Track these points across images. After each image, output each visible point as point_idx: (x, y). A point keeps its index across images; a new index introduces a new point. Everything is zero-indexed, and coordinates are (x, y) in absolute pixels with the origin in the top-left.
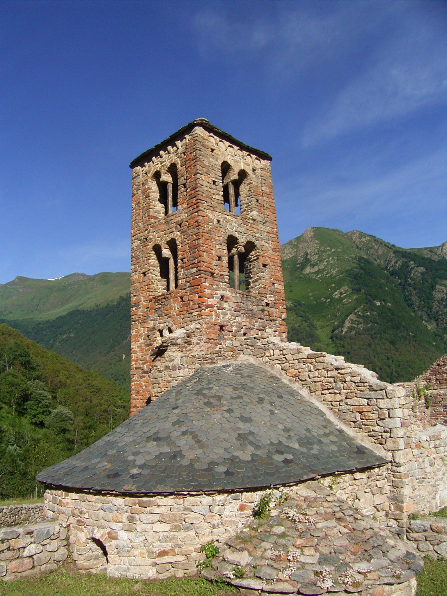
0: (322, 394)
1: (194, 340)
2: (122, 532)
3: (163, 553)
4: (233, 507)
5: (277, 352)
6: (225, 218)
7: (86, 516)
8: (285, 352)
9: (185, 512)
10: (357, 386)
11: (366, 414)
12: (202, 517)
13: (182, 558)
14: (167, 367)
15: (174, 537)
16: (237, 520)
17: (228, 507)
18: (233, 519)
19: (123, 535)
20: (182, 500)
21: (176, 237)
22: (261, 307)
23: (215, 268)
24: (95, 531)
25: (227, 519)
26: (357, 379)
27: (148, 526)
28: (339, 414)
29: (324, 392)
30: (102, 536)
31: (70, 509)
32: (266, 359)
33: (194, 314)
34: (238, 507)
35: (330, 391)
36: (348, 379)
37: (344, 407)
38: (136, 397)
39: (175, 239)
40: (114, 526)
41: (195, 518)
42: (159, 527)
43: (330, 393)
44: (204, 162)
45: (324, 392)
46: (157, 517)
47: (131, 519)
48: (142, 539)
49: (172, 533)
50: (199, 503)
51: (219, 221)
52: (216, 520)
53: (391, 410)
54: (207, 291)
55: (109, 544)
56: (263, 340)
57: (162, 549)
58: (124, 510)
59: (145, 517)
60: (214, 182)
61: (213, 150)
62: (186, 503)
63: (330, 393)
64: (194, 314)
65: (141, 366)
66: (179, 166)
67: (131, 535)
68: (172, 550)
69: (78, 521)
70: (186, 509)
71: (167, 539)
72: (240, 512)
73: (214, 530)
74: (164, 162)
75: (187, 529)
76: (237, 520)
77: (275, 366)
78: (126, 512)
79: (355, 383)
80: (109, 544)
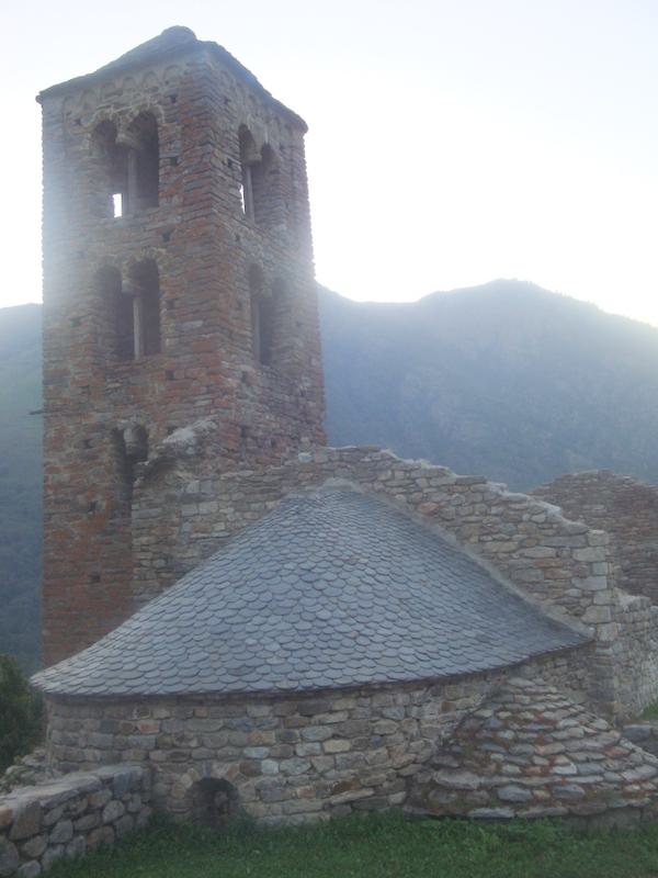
0: (480, 541)
1: (209, 450)
2: (269, 761)
3: (343, 787)
4: (433, 707)
5: (399, 474)
6: (246, 232)
7: (194, 743)
8: (414, 474)
9: (374, 719)
10: (540, 528)
11: (556, 571)
12: (397, 725)
13: (369, 792)
14: (171, 499)
15: (357, 760)
16: (439, 726)
17: (427, 708)
18: (434, 726)
19: (271, 766)
20: (369, 700)
21: (156, 257)
22: (293, 398)
23: (234, 322)
24: (215, 766)
25: (427, 726)
26: (540, 518)
27: (317, 746)
28: (508, 572)
29: (485, 538)
30: (229, 773)
31: (153, 737)
32: (378, 486)
33: (199, 403)
34: (439, 706)
35: (495, 536)
36: (525, 517)
37: (515, 560)
38: (56, 557)
39: (153, 261)
40: (253, 752)
41: (389, 727)
42: (331, 746)
43: (494, 540)
44: (217, 123)
45: (485, 538)
46: (329, 731)
47: (287, 739)
48: (306, 767)
49: (356, 753)
50: (392, 703)
51: (238, 238)
52: (414, 730)
53: (595, 565)
54: (226, 364)
55: (244, 785)
56: (374, 454)
57: (340, 780)
58: (273, 725)
59: (309, 732)
60: (230, 163)
61: (227, 101)
62: (375, 705)
63: (494, 540)
64: (199, 403)
65: (71, 498)
66: (162, 120)
67: (287, 765)
68: (356, 779)
69: (176, 755)
70: (374, 713)
71: (350, 764)
72: (442, 715)
73: (412, 744)
74: (123, 105)
75: (377, 745)
76: (439, 726)
77: (397, 496)
78: (276, 727)
79: (537, 523)
80: (244, 785)
